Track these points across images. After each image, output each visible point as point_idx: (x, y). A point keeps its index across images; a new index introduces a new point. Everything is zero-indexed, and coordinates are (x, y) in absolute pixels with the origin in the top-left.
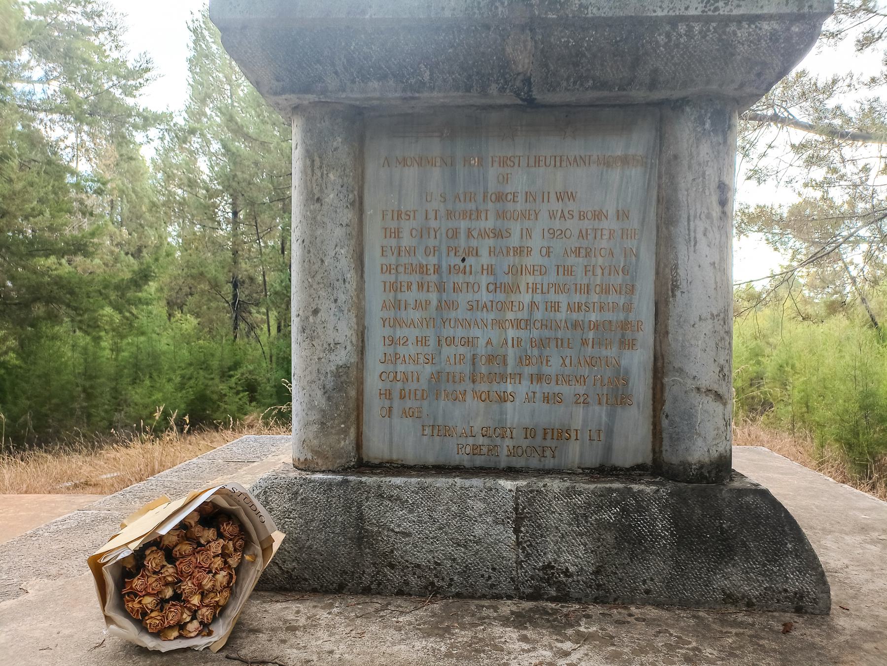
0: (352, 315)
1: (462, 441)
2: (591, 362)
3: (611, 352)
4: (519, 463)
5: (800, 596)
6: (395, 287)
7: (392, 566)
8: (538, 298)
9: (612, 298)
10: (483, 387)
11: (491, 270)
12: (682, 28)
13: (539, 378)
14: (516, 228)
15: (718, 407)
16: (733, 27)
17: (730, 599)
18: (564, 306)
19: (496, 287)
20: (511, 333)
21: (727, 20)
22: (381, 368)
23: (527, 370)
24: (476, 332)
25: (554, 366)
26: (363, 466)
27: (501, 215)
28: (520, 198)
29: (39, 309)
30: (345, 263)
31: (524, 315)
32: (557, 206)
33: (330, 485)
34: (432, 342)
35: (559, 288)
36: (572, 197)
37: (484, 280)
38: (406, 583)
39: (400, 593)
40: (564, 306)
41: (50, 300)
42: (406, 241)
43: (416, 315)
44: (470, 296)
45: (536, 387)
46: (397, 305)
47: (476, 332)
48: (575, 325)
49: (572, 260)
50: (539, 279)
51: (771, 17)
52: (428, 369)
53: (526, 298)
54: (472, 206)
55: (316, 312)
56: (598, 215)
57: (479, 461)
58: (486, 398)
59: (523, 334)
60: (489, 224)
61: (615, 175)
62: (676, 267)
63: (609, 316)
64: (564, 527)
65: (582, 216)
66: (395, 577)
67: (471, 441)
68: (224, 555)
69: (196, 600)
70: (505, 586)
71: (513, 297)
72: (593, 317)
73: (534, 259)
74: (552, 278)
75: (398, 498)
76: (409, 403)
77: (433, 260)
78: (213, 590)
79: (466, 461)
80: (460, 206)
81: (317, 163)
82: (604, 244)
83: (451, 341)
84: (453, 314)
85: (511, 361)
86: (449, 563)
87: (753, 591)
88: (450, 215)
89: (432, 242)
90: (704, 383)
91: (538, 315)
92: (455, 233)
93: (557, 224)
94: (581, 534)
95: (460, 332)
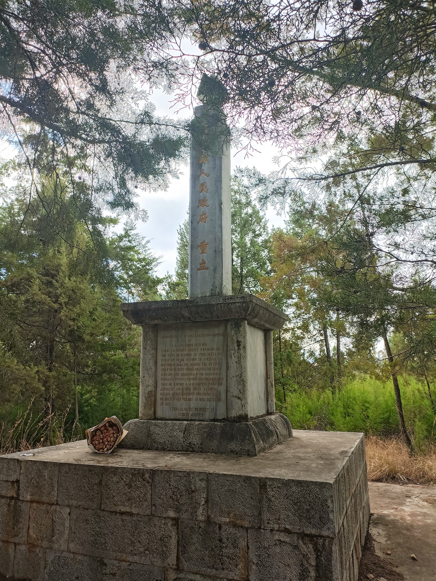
0: (153, 377)
1: (180, 412)
2: (211, 389)
3: (216, 387)
4: (194, 418)
5: (248, 451)
6: (164, 370)
8: (198, 372)
9: (216, 371)
10: (185, 397)
11: (187, 365)
12: (219, 306)
13: (198, 394)
14: (192, 353)
15: (239, 401)
16: (230, 305)
17: (232, 451)
18: (204, 374)
19: (188, 369)
20: (192, 381)
21: (229, 304)
22: (161, 392)
23: (196, 392)
24: (183, 382)
25: (202, 391)
26: (155, 419)
27: (189, 350)
28: (194, 345)
29: (105, 376)
30: (152, 364)
31: (195, 376)
32: (202, 347)
33: (144, 423)
34: (173, 384)
35: (203, 369)
36: (206, 345)
37: (185, 367)
39: (156, 450)
40: (204, 374)
41: (111, 371)
42: (167, 358)
43: (169, 377)
44: (182, 372)
45: (198, 396)
46: (165, 375)
47: (183, 382)
48: (207, 379)
49: (206, 361)
50: (198, 367)
51: (238, 302)
52: (172, 392)
53: (195, 372)
54: (182, 348)
55: (144, 377)
56: (212, 349)
58: (185, 399)
59: (194, 382)
61: (216, 338)
63: (215, 376)
64: (195, 433)
65: (208, 350)
66: (155, 445)
67: (182, 412)
68: (113, 434)
69: (106, 443)
70: (180, 448)
71: (192, 372)
72: (211, 377)
73: (197, 361)
74: (201, 366)
76: (167, 401)
77: (173, 362)
78: (110, 441)
79: (180, 417)
80: (180, 348)
82: (214, 357)
83: (177, 384)
84: (178, 377)
85: (191, 389)
87: (237, 449)
88: (177, 350)
89: (173, 358)
90: (235, 394)
91: (198, 377)
92: (179, 355)
93: (202, 352)
95: (179, 382)
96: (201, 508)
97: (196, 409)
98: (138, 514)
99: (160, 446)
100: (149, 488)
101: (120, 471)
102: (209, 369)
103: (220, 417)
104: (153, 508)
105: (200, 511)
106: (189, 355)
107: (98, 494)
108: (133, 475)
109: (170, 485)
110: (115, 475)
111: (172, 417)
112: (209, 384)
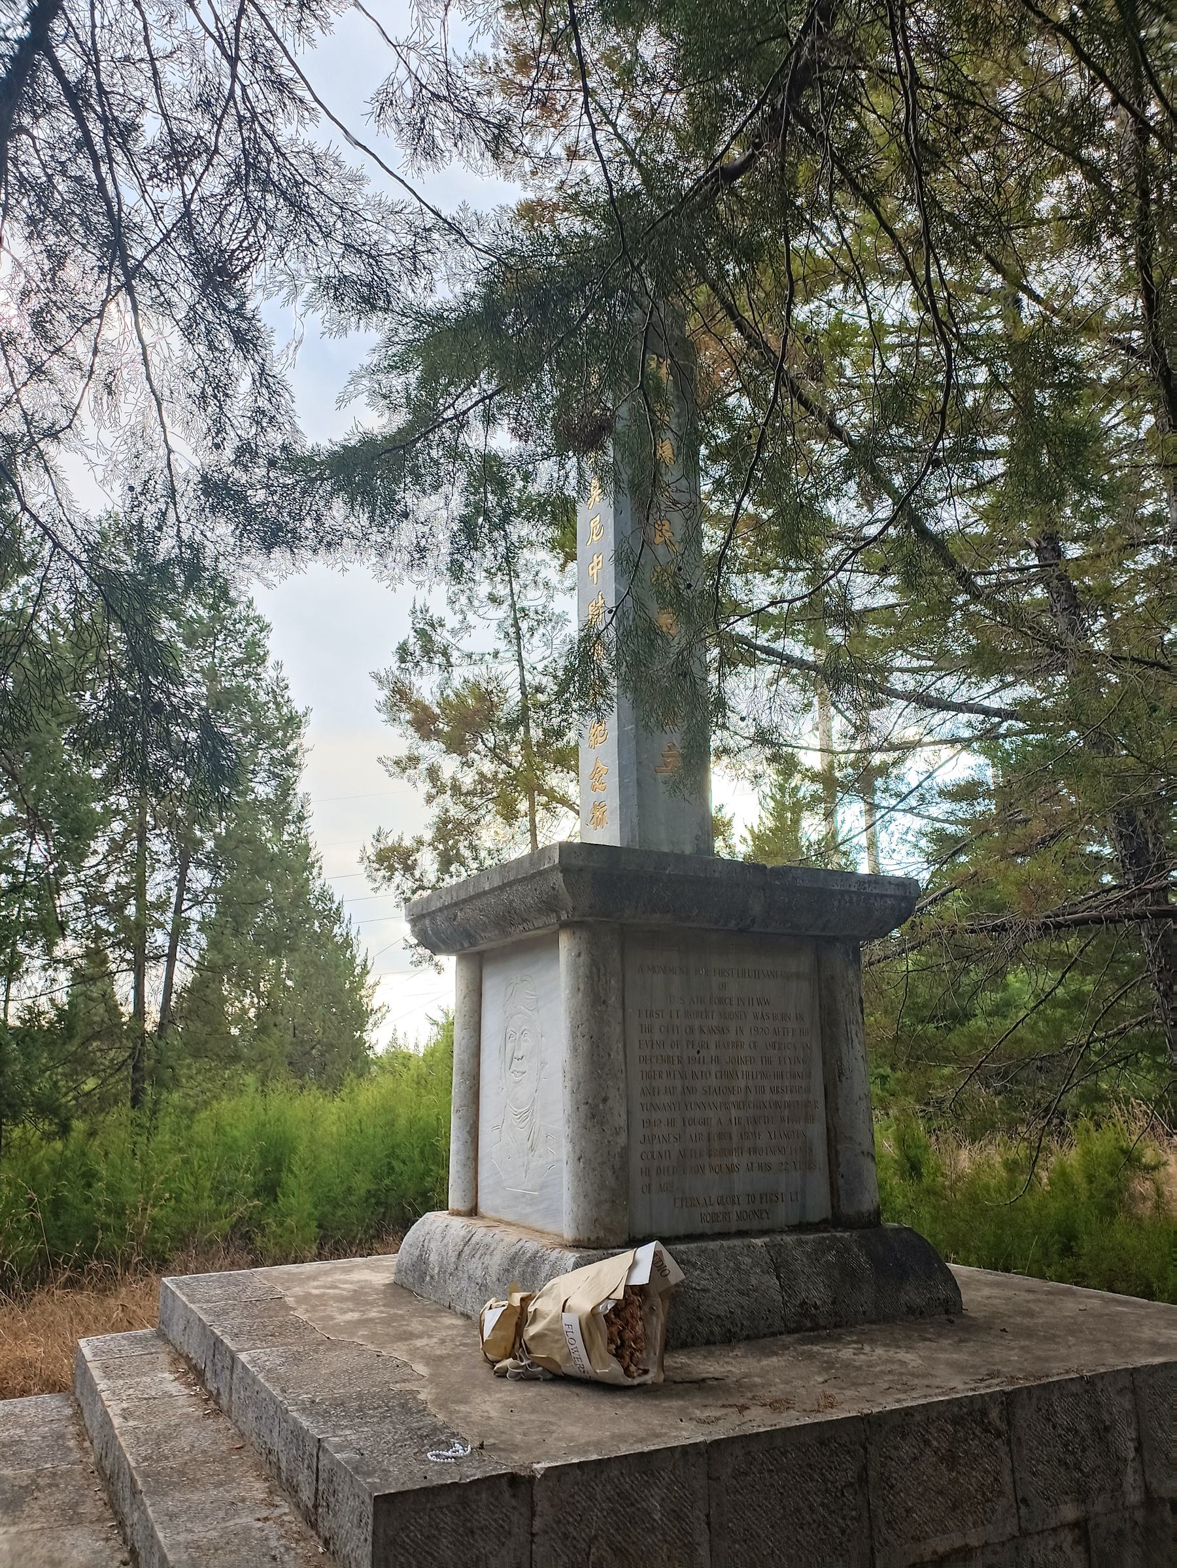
4: (745, 1226)
6: (649, 1075)
7: (700, 1320)
8: (751, 1083)
11: (717, 1060)
13: (754, 1150)
17: (911, 1310)
18: (767, 1090)
20: (734, 1113)
24: (710, 1113)
28: (734, 1002)
35: (764, 1075)
36: (767, 1002)
37: (714, 1068)
38: (712, 1333)
39: (708, 1343)
40: (767, 1090)
43: (666, 1099)
47: (710, 1113)
48: (776, 1105)
53: (742, 1083)
55: (605, 1100)
57: (717, 1227)
60: (714, 1022)
62: (841, 1059)
66: (703, 1329)
70: (778, 1324)
75: (689, 1262)
79: (706, 1228)
81: (602, 970)
86: (739, 1311)
91: (751, 1097)
94: (818, 1274)
96: (1130, 1471)
97: (751, 1198)
98: (987, 1544)
99: (716, 1329)
100: (1003, 1450)
101: (918, 1418)
102: (781, 1076)
103: (814, 1216)
104: (1023, 1510)
105: (1130, 1477)
106: (723, 1031)
107: (858, 1519)
108: (956, 1421)
109: (1054, 1427)
110: (903, 1438)
111: (682, 1231)
112: (783, 1120)
